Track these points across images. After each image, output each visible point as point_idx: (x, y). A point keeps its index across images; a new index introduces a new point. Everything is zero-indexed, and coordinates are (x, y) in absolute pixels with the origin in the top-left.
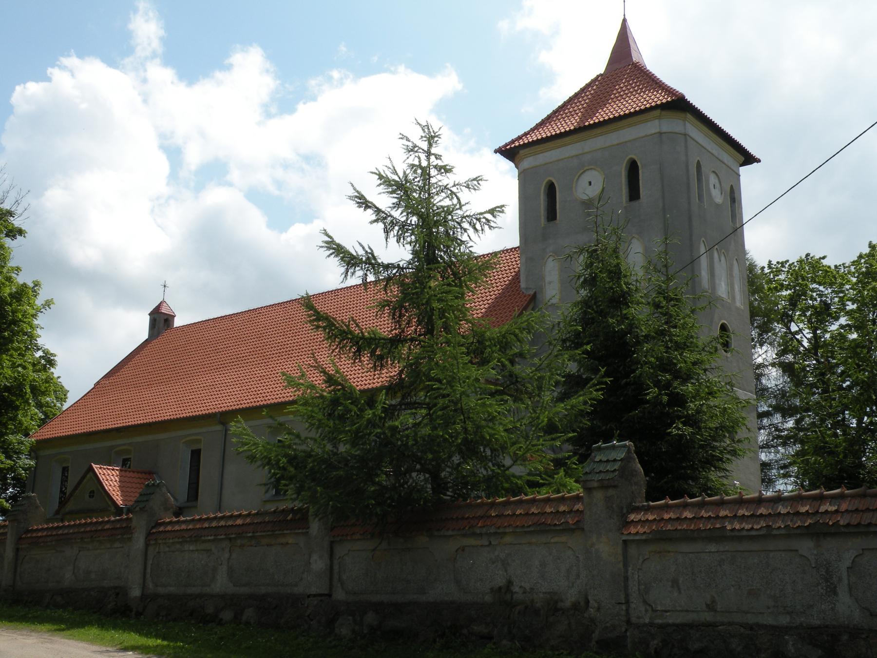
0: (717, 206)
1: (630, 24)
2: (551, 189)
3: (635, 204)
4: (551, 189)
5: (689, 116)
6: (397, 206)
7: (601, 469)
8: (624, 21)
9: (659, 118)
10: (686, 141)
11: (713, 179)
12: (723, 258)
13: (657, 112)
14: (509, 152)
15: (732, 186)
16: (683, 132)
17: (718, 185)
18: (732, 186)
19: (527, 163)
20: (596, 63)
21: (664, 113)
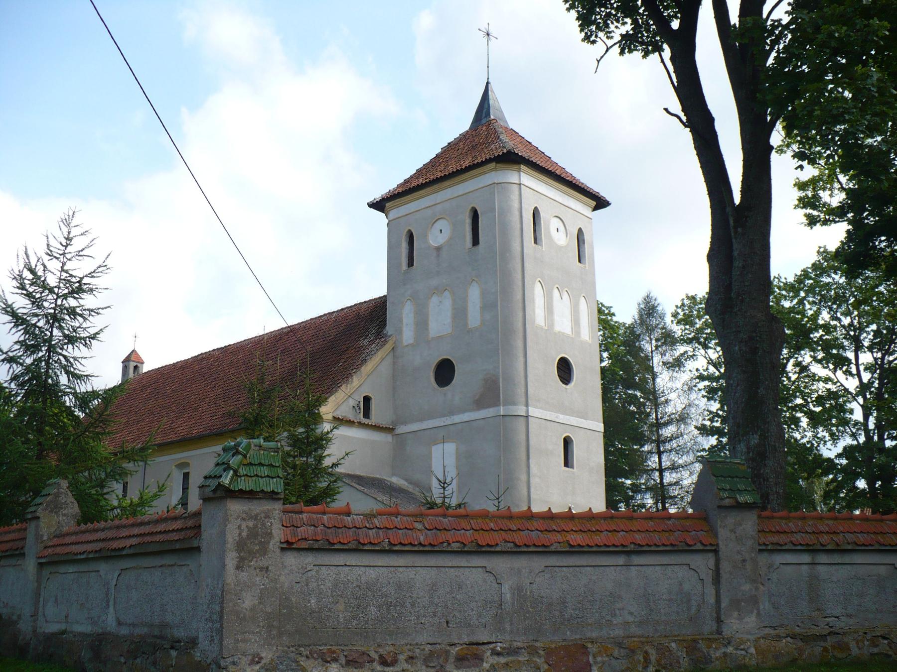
0: (560, 248)
1: (493, 86)
2: (411, 237)
3: (477, 247)
4: (411, 237)
5: (523, 167)
6: (792, 301)
7: (651, 523)
8: (488, 83)
9: (495, 169)
10: (520, 189)
11: (555, 223)
12: (565, 296)
13: (493, 165)
14: (379, 205)
15: (580, 230)
16: (517, 182)
17: (562, 228)
18: (580, 230)
19: (393, 214)
20: (464, 123)
21: (499, 165)
